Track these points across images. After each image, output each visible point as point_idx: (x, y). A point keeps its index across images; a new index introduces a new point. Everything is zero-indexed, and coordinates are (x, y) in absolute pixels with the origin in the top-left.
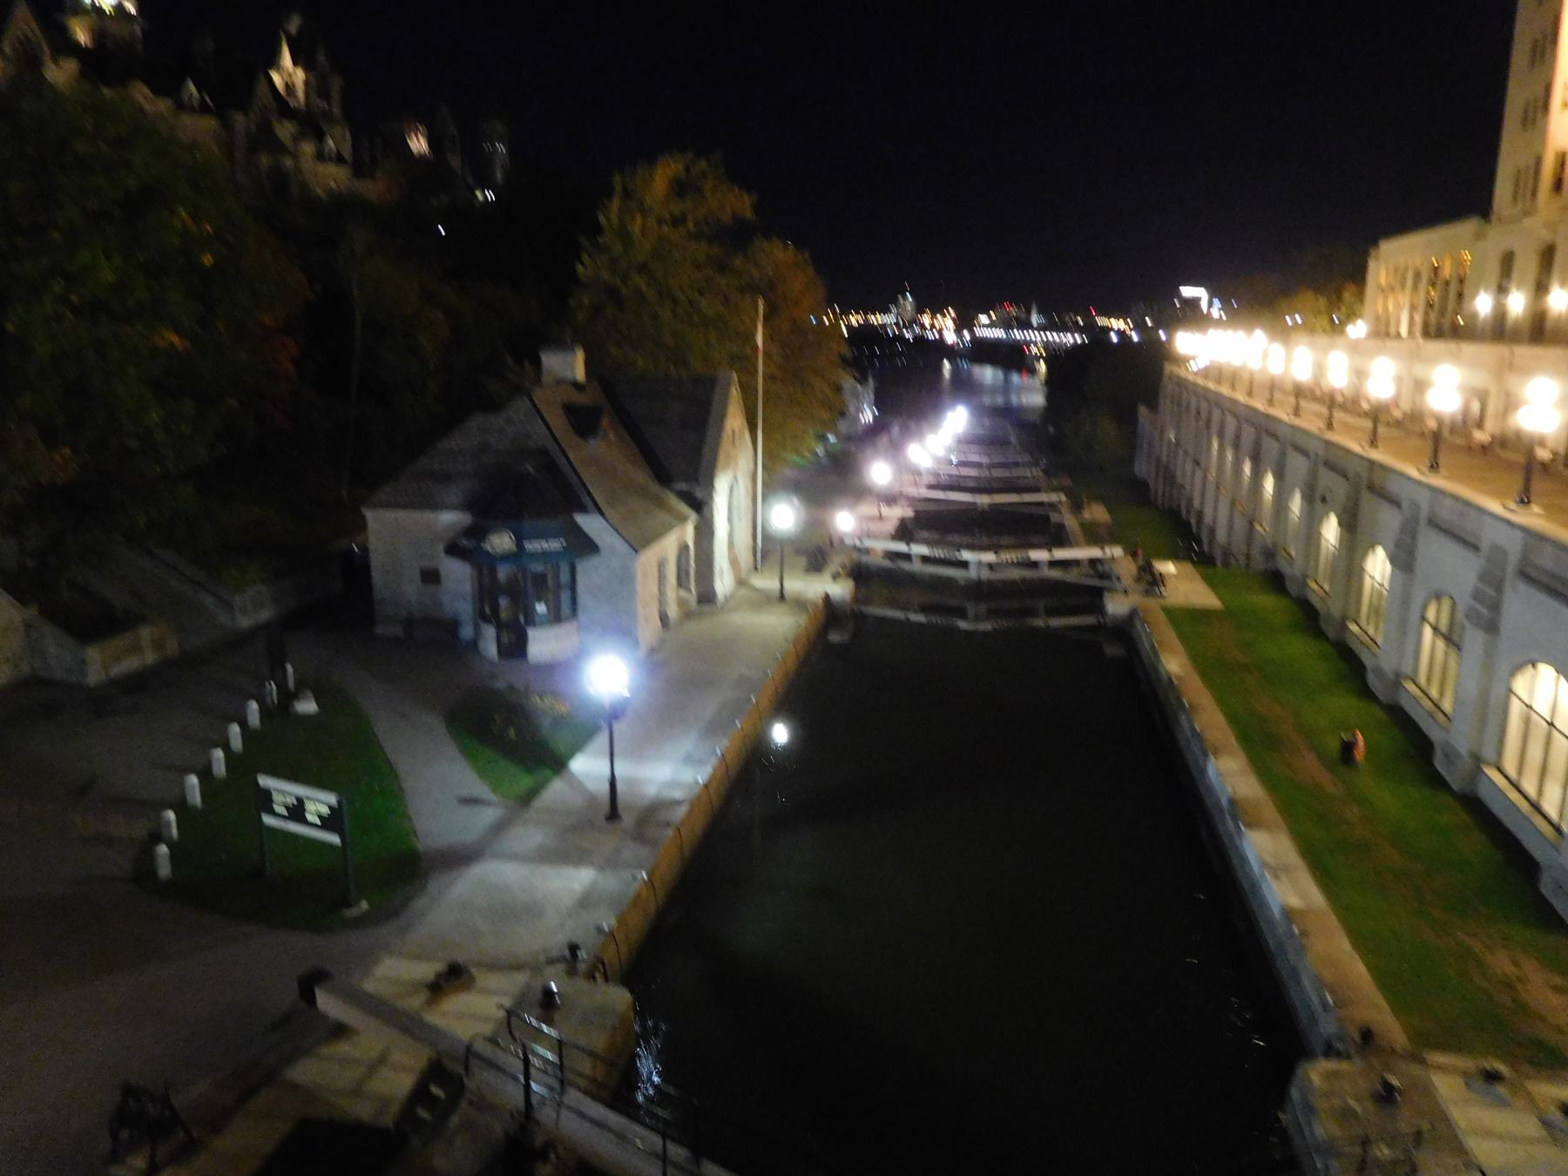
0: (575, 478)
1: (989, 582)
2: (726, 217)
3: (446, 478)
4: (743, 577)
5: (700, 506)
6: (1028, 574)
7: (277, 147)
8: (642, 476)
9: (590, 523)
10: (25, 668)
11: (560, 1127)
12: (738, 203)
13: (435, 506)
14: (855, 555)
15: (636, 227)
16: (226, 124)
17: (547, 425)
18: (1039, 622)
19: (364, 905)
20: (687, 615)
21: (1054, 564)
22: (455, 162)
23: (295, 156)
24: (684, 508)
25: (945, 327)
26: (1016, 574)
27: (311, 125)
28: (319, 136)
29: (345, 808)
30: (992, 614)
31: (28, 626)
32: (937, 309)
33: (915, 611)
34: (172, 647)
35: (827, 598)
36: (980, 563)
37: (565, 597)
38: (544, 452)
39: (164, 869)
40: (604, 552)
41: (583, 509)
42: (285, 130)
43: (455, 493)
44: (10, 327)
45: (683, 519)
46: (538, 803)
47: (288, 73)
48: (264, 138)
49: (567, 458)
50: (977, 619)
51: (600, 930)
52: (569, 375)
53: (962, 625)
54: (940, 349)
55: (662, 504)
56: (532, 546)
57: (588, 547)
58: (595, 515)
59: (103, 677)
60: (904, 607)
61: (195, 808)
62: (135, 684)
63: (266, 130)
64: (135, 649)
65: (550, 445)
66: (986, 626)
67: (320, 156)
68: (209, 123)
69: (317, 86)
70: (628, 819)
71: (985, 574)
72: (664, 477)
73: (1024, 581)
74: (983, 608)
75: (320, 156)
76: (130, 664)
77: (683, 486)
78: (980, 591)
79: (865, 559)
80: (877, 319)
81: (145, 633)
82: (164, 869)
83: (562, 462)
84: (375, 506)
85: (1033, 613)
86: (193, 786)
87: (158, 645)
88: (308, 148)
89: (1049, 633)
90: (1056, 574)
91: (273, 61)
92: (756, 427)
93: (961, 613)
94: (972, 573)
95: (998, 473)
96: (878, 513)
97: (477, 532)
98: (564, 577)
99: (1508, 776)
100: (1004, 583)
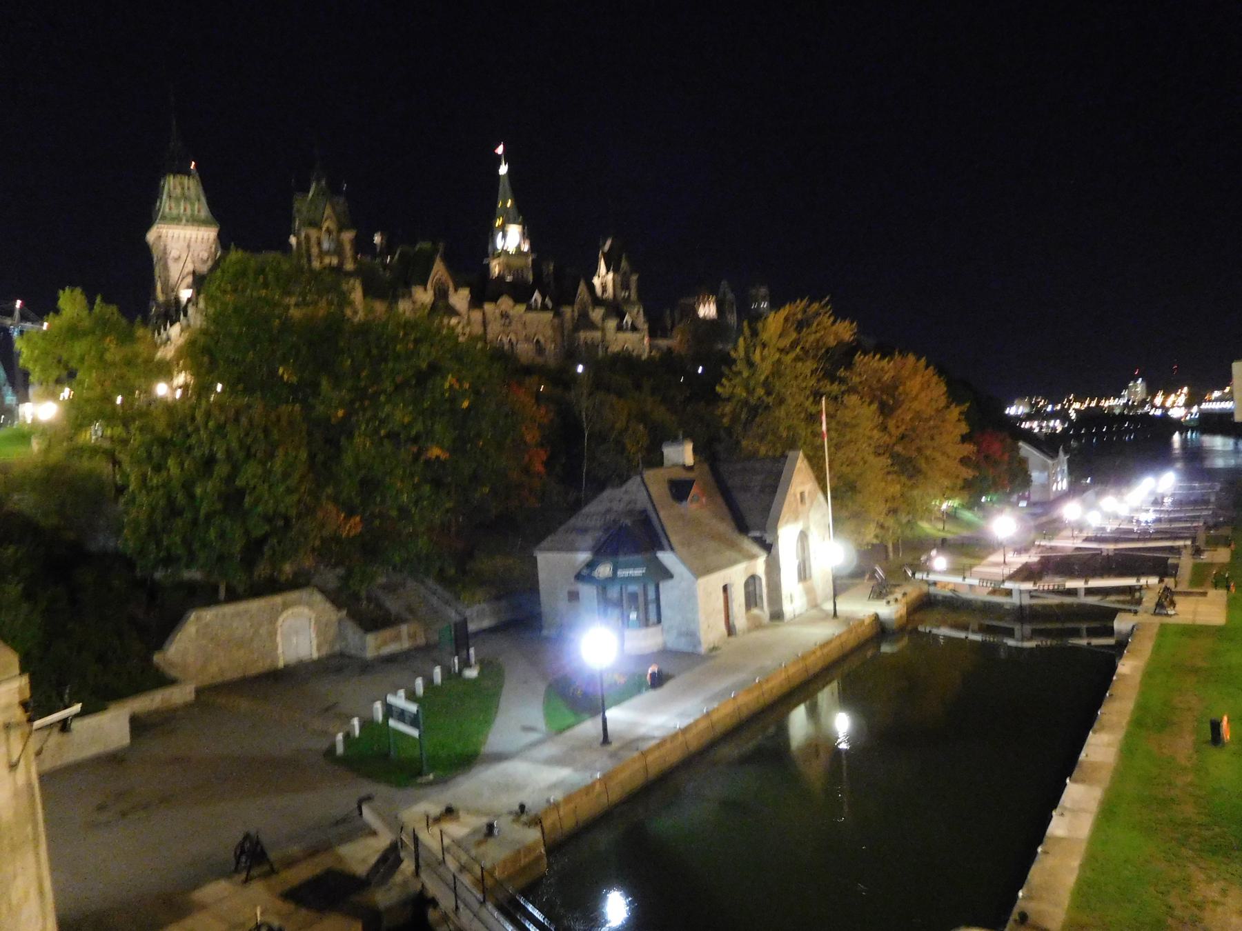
0: (660, 527)
1: (1031, 607)
2: (831, 341)
3: (583, 531)
4: (819, 601)
5: (768, 547)
6: (1068, 600)
7: (592, 326)
8: (725, 527)
9: (666, 558)
10: (337, 648)
11: (435, 876)
12: (845, 331)
13: (572, 548)
14: (925, 588)
15: (757, 357)
16: (558, 314)
17: (649, 496)
18: (1083, 642)
19: (431, 777)
20: (756, 625)
21: (1090, 592)
22: (732, 319)
23: (603, 330)
24: (755, 549)
25: (1176, 405)
26: (1055, 600)
27: (615, 309)
28: (621, 316)
29: (420, 715)
30: (1036, 633)
31: (340, 622)
32: (1170, 389)
33: (974, 632)
34: (421, 641)
35: (877, 617)
36: (1021, 592)
37: (652, 608)
38: (644, 511)
39: (340, 749)
40: (676, 578)
41: (662, 548)
42: (597, 314)
43: (589, 540)
44: (983, 499)
45: (753, 557)
46: (568, 733)
47: (603, 278)
48: (583, 322)
49: (657, 514)
50: (1023, 639)
51: (548, 801)
52: (681, 461)
53: (1011, 642)
54: (1168, 425)
55: (733, 545)
56: (622, 573)
57: (667, 574)
58: (668, 552)
59: (376, 654)
60: (965, 628)
61: (377, 723)
62: (391, 659)
63: (584, 315)
64: (397, 638)
65: (650, 507)
66: (977, 637)
67: (620, 328)
68: (548, 316)
69: (623, 284)
70: (615, 745)
71: (1026, 601)
72: (743, 527)
73: (1061, 606)
74: (1028, 628)
75: (620, 328)
76: (392, 648)
77: (757, 534)
78: (1022, 614)
79: (932, 590)
80: (1106, 404)
81: (404, 629)
82: (340, 749)
83: (653, 516)
84: (540, 550)
85: (1076, 633)
86: (377, 708)
87: (412, 636)
88: (612, 324)
89: (1089, 649)
90: (1093, 600)
91: (594, 270)
92: (827, 493)
93: (1010, 633)
94: (1015, 600)
95: (1164, 526)
96: (1003, 560)
97: (591, 565)
98: (651, 595)
99: (725, 616)
100: (1044, 607)
